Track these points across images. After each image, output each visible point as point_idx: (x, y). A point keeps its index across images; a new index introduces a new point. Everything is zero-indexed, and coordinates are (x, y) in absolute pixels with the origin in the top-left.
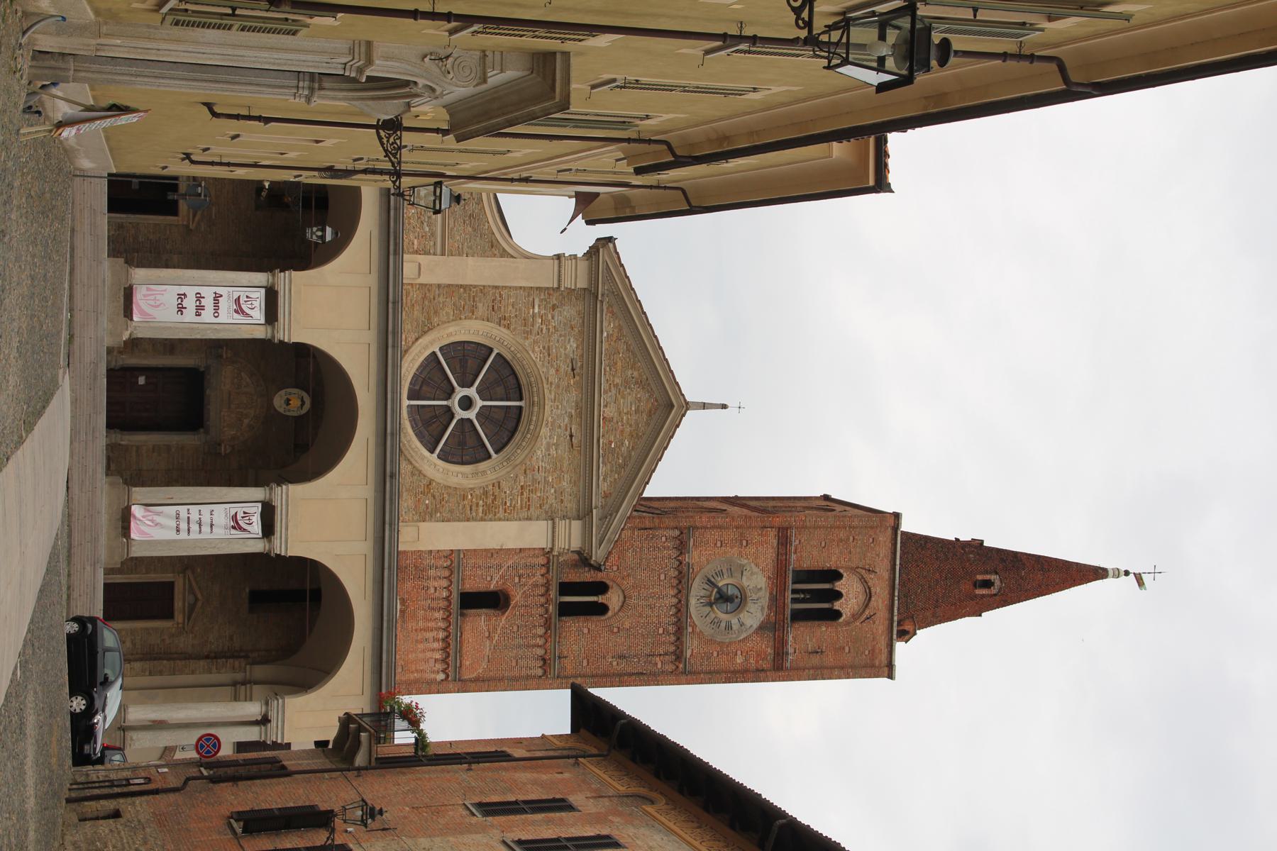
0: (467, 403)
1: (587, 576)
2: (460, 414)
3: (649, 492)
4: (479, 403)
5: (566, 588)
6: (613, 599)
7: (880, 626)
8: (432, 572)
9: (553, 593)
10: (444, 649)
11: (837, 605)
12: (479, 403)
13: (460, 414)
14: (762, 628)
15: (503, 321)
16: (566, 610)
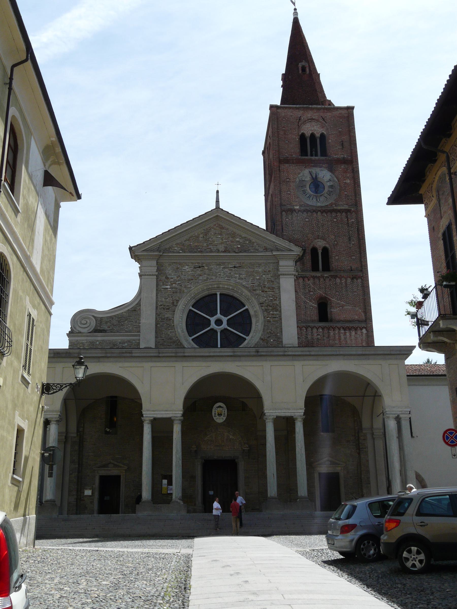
0: (219, 322)
1: (308, 257)
2: (225, 325)
3: (263, 225)
4: (219, 316)
5: (315, 268)
6: (320, 244)
7: (328, 115)
8: (309, 337)
9: (318, 274)
10: (350, 329)
11: (318, 135)
12: (219, 316)
13: (225, 325)
14: (331, 170)
15: (175, 304)
16: (327, 268)
